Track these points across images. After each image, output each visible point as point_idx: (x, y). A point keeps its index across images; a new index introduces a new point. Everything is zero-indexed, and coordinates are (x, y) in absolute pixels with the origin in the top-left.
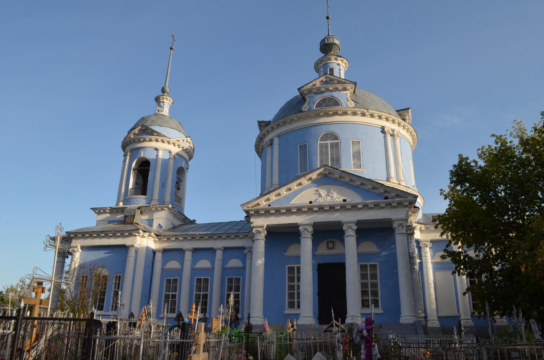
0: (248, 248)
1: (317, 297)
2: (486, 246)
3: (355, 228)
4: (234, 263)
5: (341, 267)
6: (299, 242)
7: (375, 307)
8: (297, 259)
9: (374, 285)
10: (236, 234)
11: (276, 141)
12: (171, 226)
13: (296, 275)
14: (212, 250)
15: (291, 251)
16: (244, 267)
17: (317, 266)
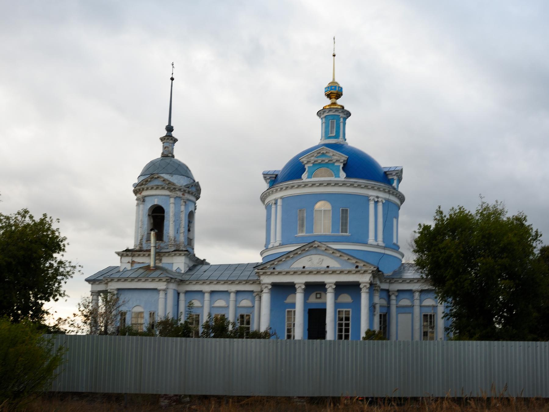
0: (256, 292)
1: (307, 332)
2: (150, 403)
3: (334, 287)
4: (245, 303)
5: (323, 312)
6: (295, 294)
7: (375, 332)
8: (293, 305)
9: (347, 325)
10: (246, 281)
11: (279, 202)
12: (187, 269)
13: (293, 316)
14: (227, 292)
15: (289, 300)
16: (253, 307)
17: (307, 311)
